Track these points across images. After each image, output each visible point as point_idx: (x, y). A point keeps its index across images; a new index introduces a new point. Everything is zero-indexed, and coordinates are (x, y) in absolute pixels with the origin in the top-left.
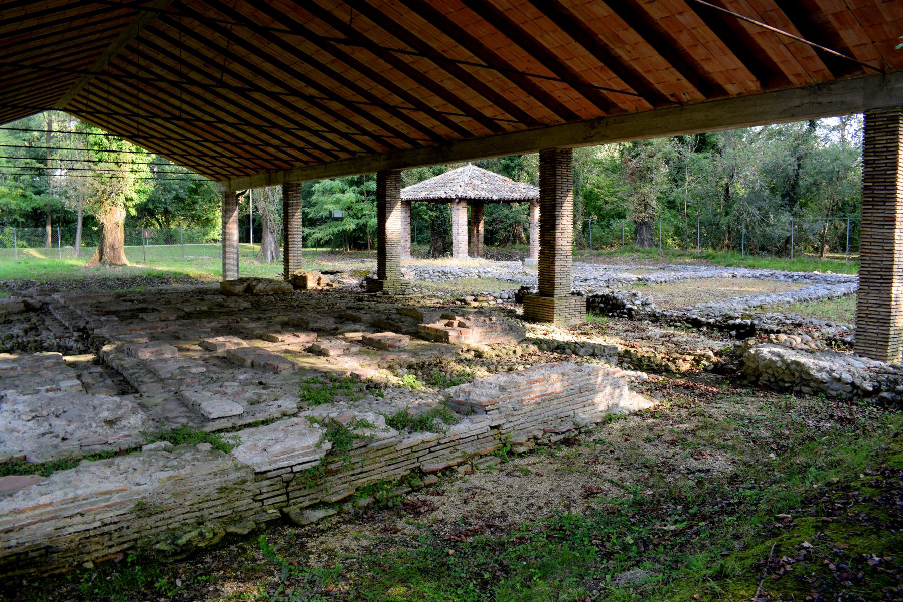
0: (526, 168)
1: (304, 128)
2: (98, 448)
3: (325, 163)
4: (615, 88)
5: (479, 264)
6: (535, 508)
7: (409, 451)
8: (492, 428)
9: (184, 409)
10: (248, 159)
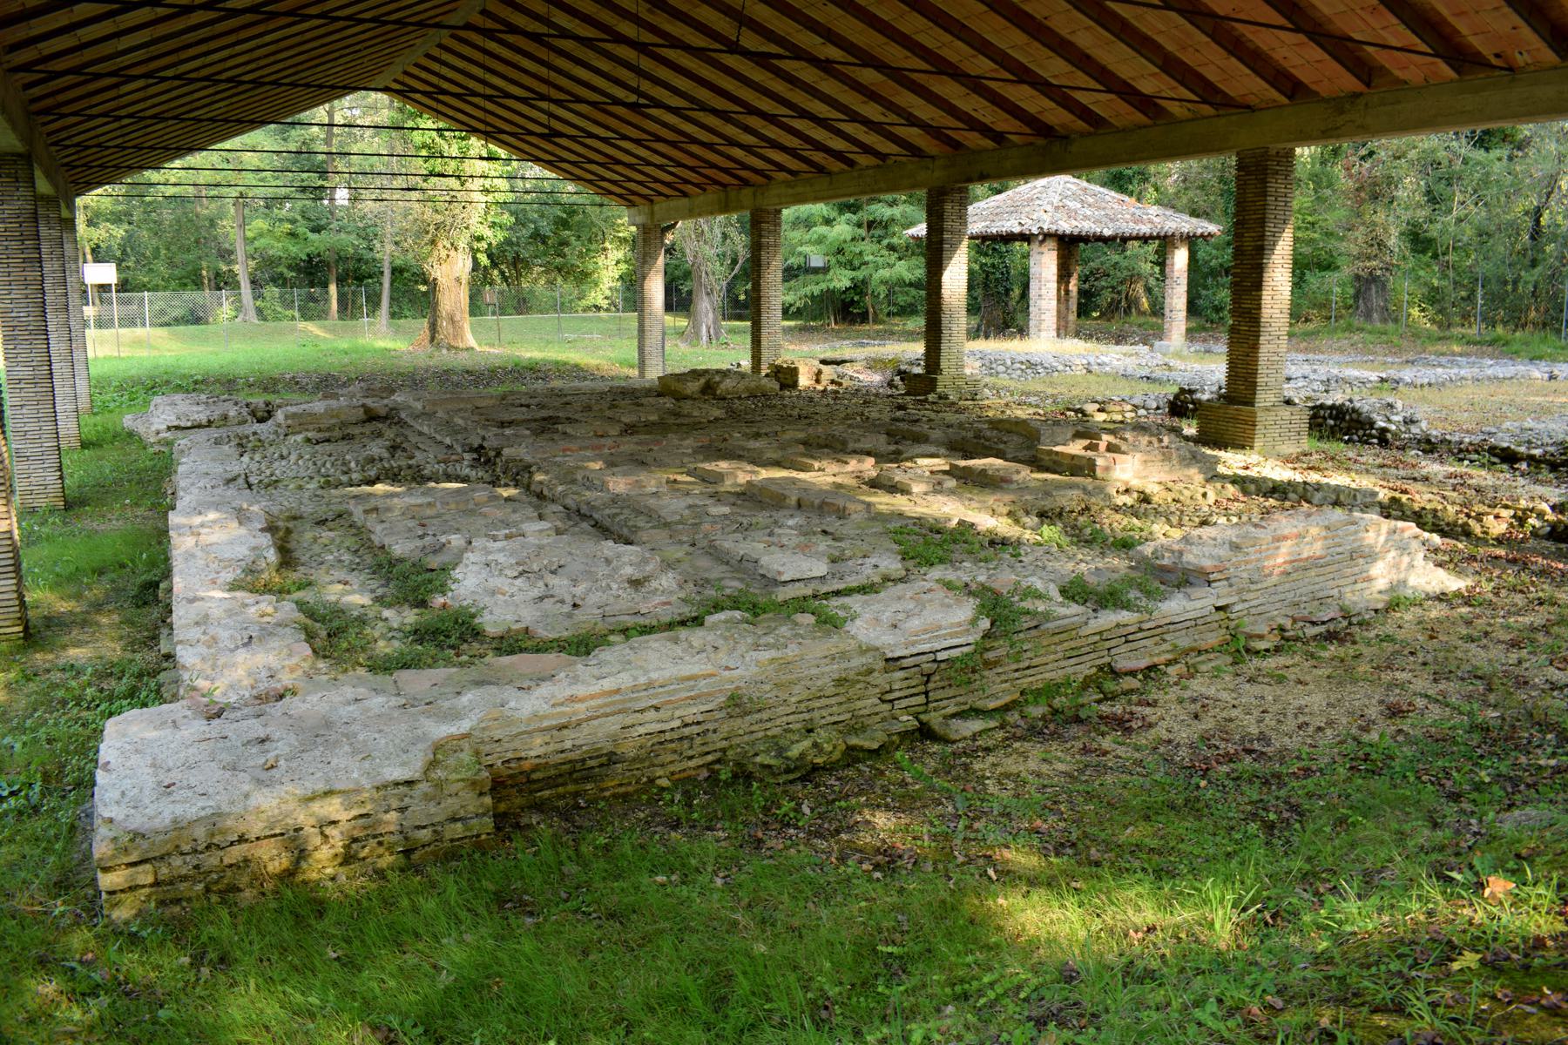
0: (1152, 180)
1: (804, 114)
2: (629, 621)
3: (829, 173)
4: (1394, 43)
5: (1077, 349)
6: (1311, 729)
7: (1097, 638)
8: (1218, 609)
9: (725, 568)
10: (692, 169)
